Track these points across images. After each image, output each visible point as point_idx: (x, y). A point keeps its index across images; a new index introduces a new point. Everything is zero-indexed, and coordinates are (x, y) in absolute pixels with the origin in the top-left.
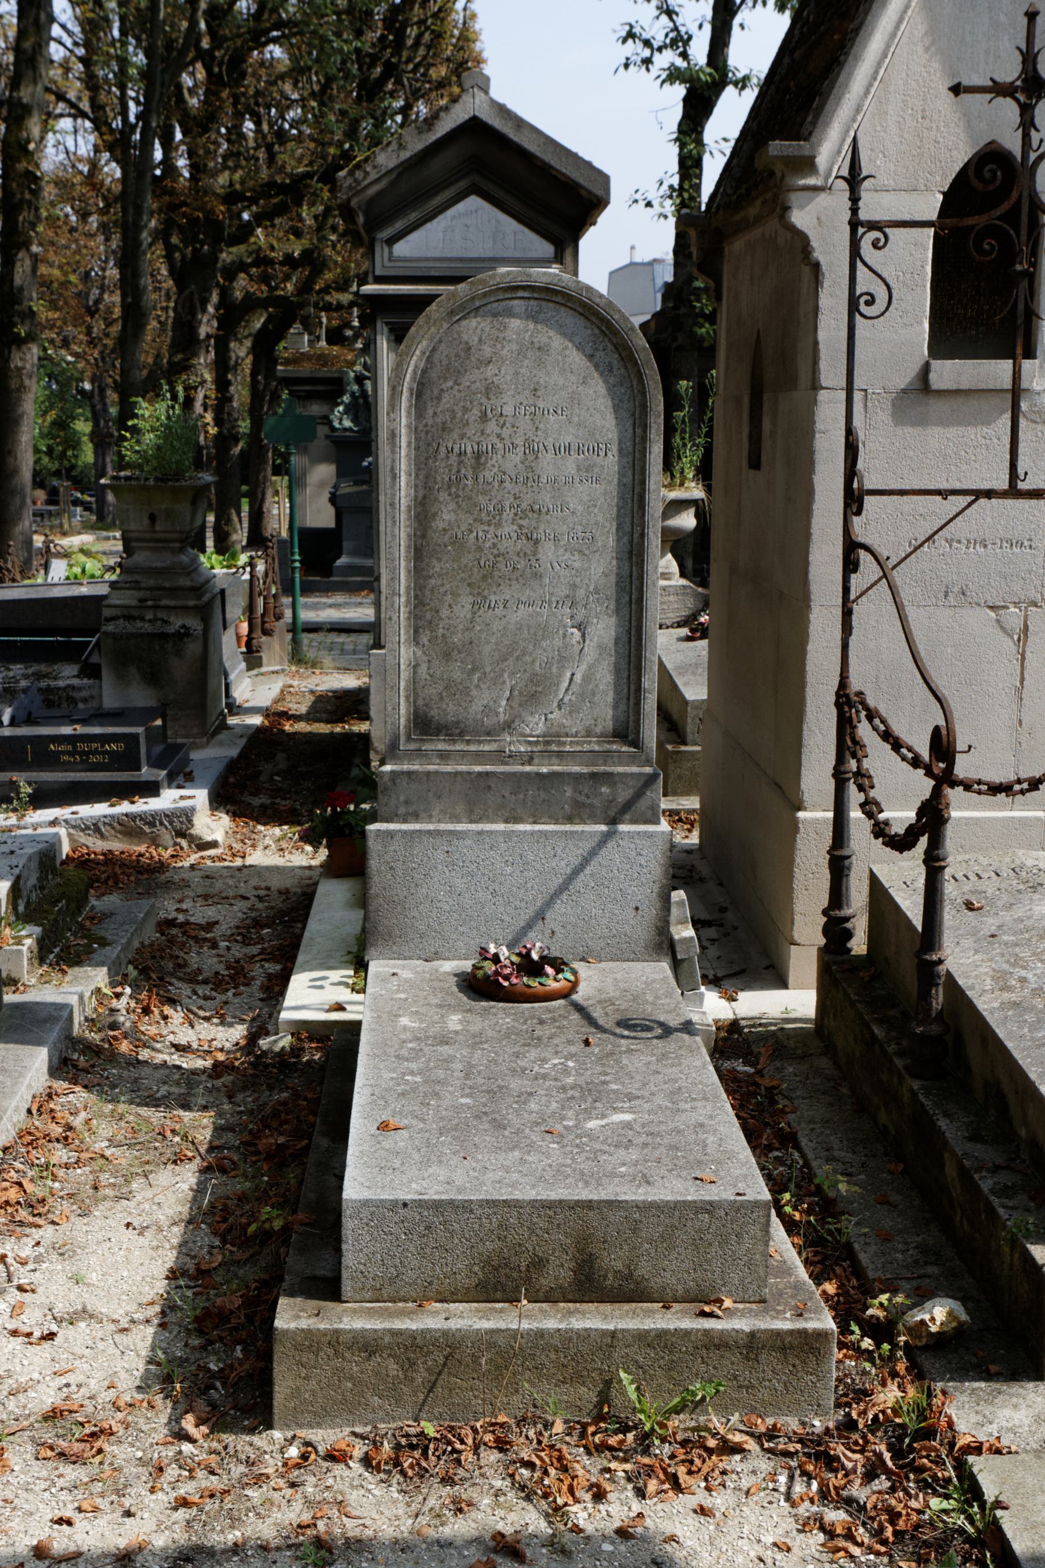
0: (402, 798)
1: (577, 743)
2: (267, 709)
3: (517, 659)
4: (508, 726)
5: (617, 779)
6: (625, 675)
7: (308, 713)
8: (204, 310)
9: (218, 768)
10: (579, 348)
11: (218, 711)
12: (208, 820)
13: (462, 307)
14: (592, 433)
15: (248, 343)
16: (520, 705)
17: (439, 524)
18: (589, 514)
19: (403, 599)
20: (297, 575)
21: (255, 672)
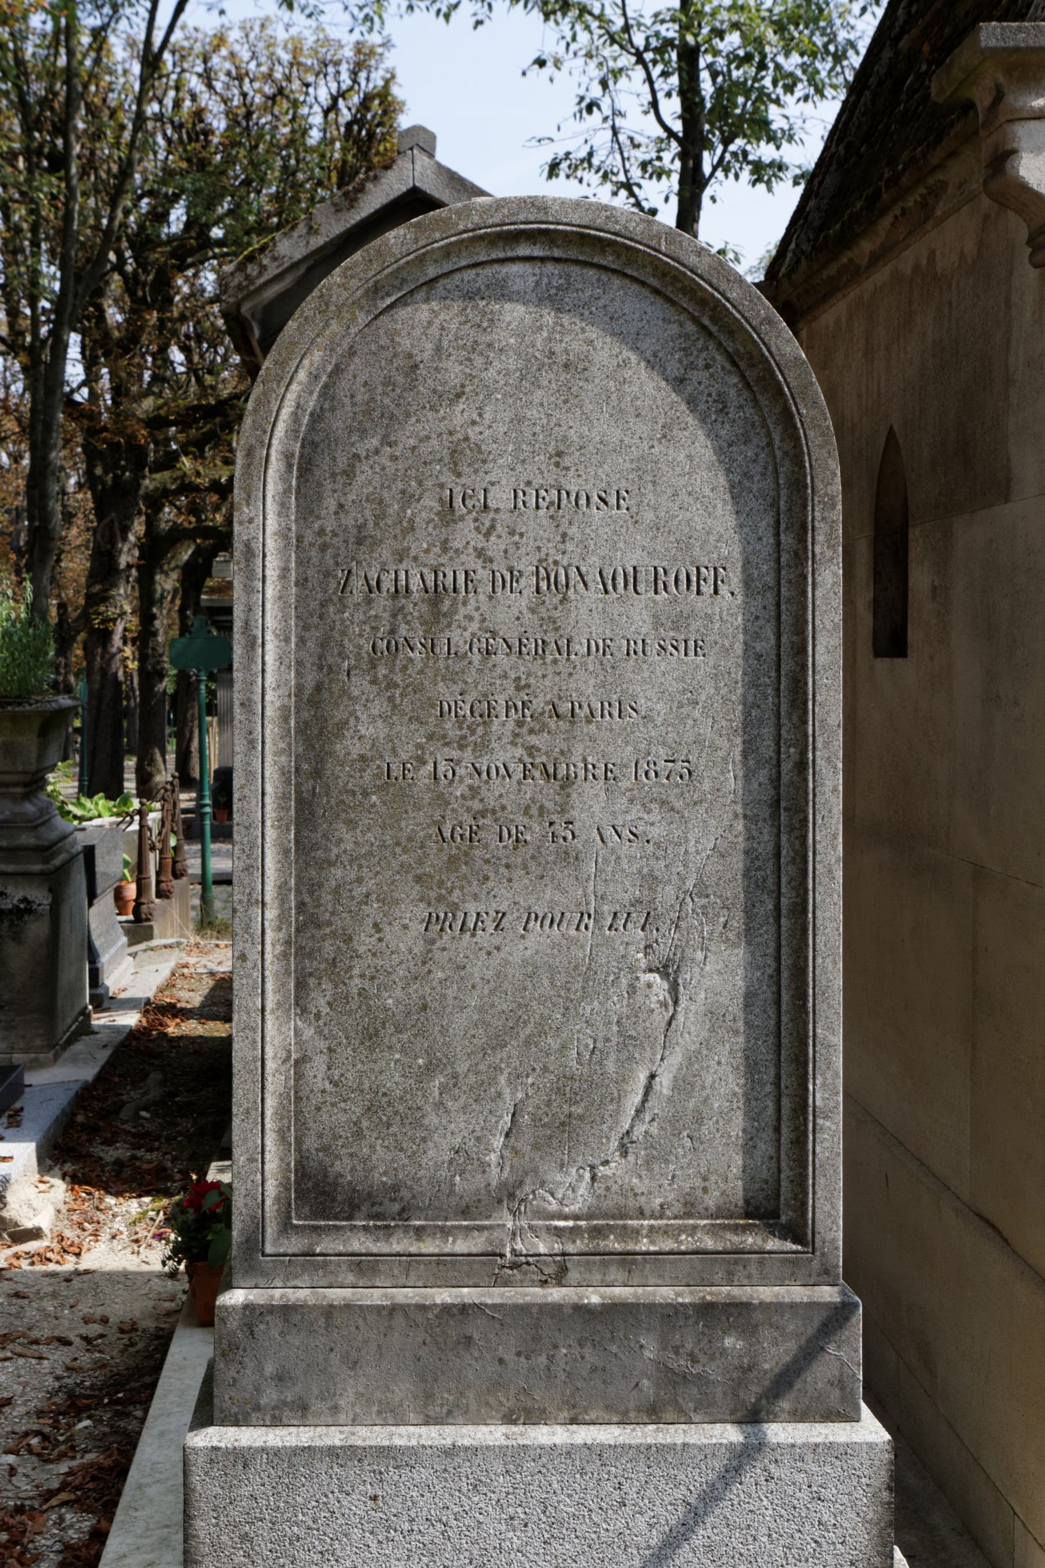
0: (269, 1369)
1: (666, 1232)
2: (148, 1002)
3: (527, 1043)
4: (509, 1194)
5: (758, 1316)
6: (769, 1075)
7: (203, 1005)
8: (125, 539)
9: (61, 1101)
10: (654, 363)
11: (77, 1009)
12: (31, 1192)
13: (399, 277)
14: (684, 545)
15: (175, 575)
16: (536, 1147)
17: (350, 746)
18: (682, 721)
19: (271, 914)
20: (208, 822)
21: (143, 946)
